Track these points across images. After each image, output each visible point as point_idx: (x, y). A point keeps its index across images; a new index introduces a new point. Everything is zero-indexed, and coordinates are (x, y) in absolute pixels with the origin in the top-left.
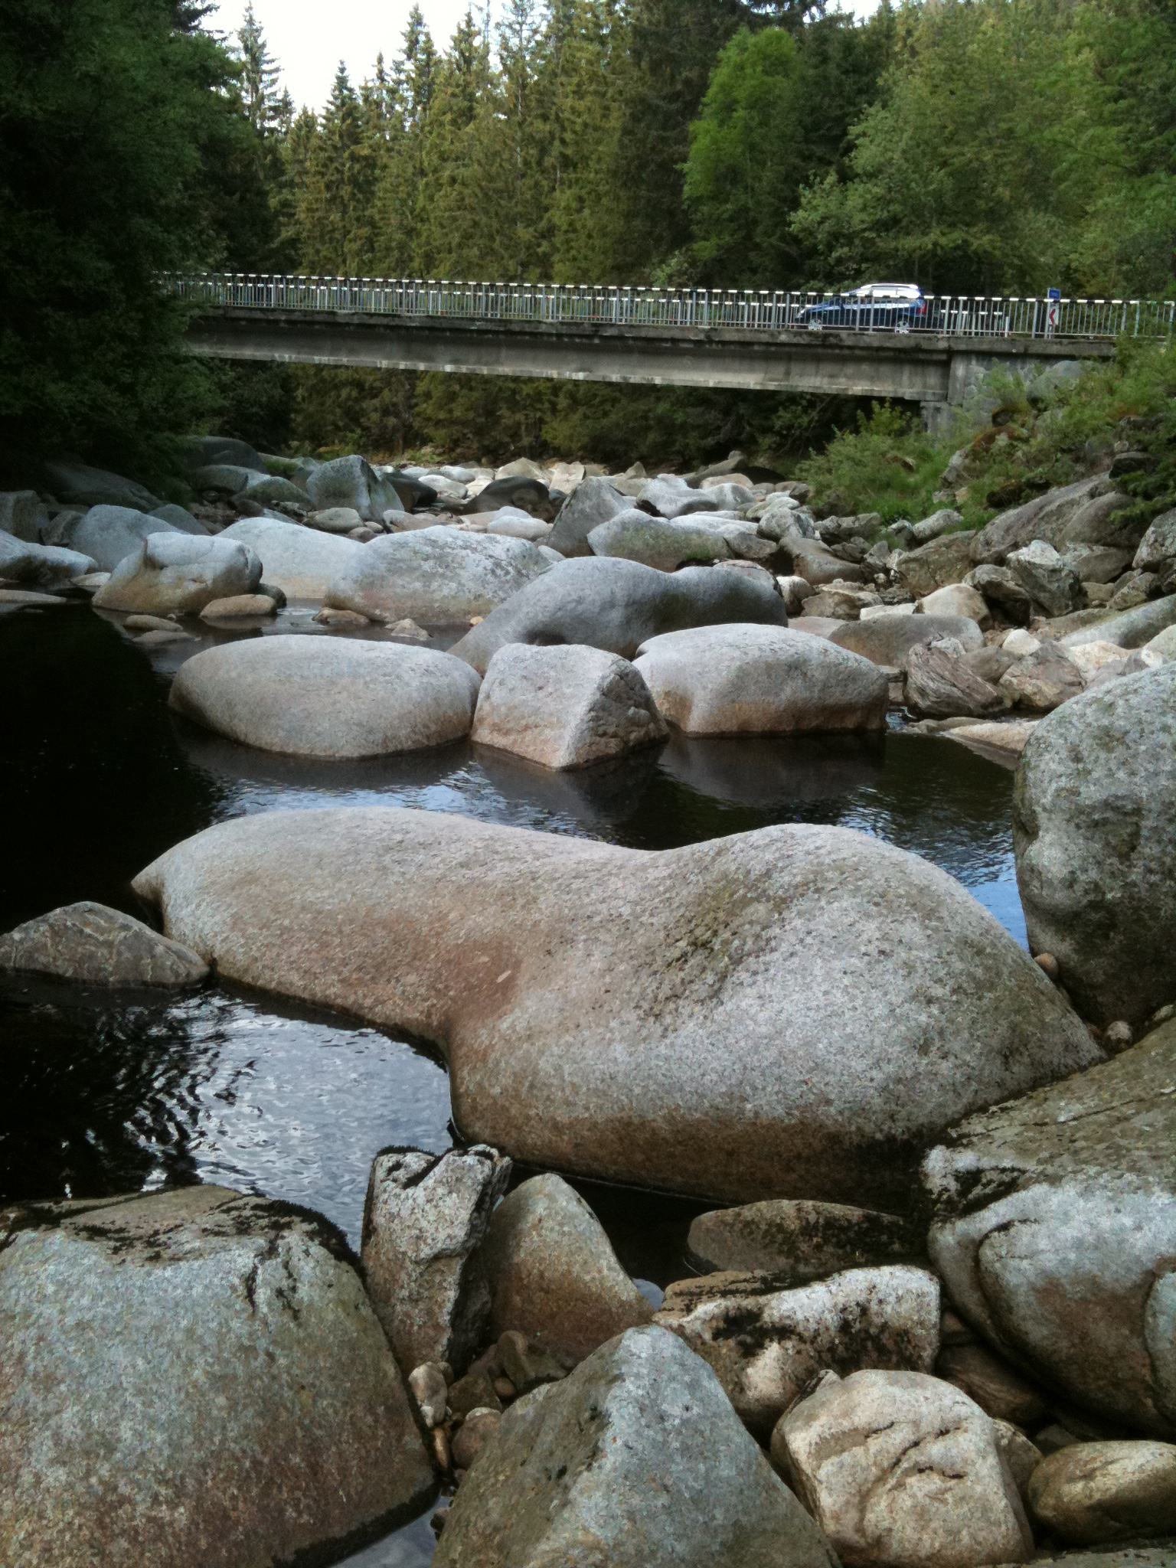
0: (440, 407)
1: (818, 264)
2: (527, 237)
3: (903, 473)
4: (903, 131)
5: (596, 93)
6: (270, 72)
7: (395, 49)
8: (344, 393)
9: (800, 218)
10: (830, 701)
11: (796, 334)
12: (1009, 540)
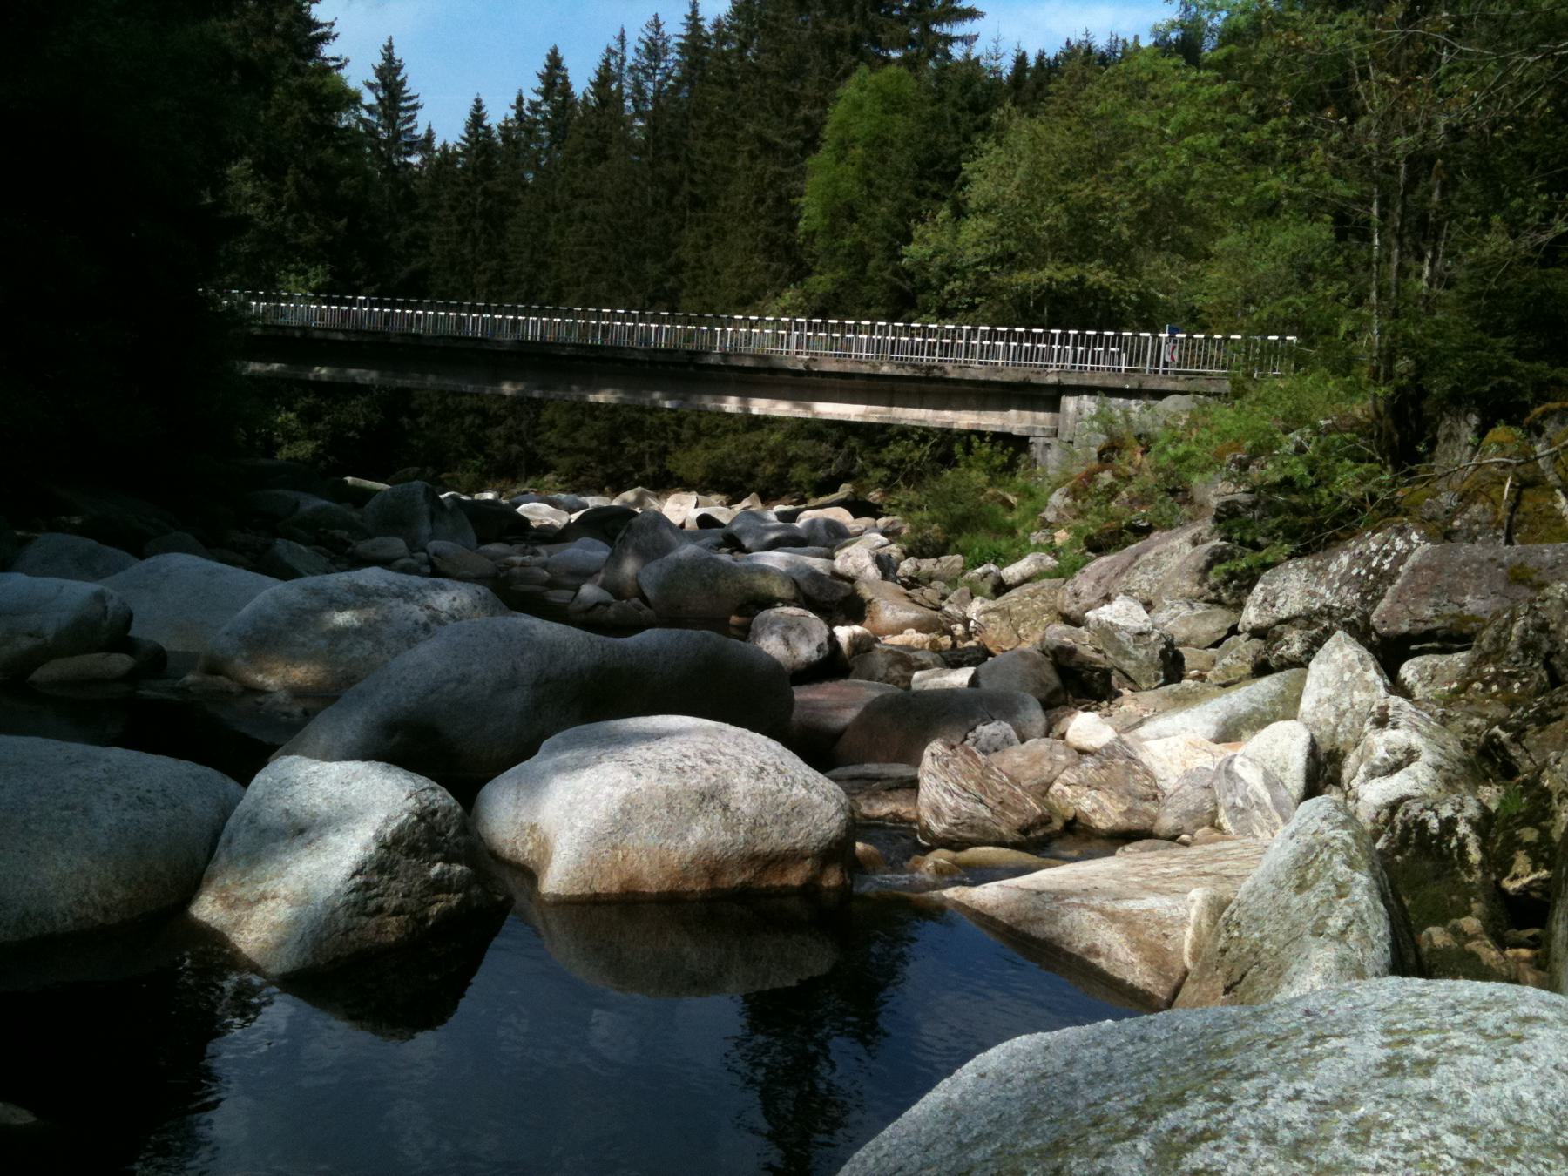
0: (565, 436)
1: (930, 298)
2: (656, 272)
3: (1001, 510)
4: (1015, 167)
5: (726, 135)
6: (407, 109)
7: (531, 88)
8: (468, 420)
9: (913, 252)
10: (763, 847)
11: (898, 366)
12: (1100, 592)
